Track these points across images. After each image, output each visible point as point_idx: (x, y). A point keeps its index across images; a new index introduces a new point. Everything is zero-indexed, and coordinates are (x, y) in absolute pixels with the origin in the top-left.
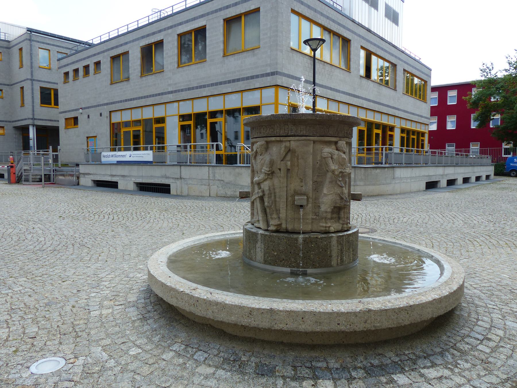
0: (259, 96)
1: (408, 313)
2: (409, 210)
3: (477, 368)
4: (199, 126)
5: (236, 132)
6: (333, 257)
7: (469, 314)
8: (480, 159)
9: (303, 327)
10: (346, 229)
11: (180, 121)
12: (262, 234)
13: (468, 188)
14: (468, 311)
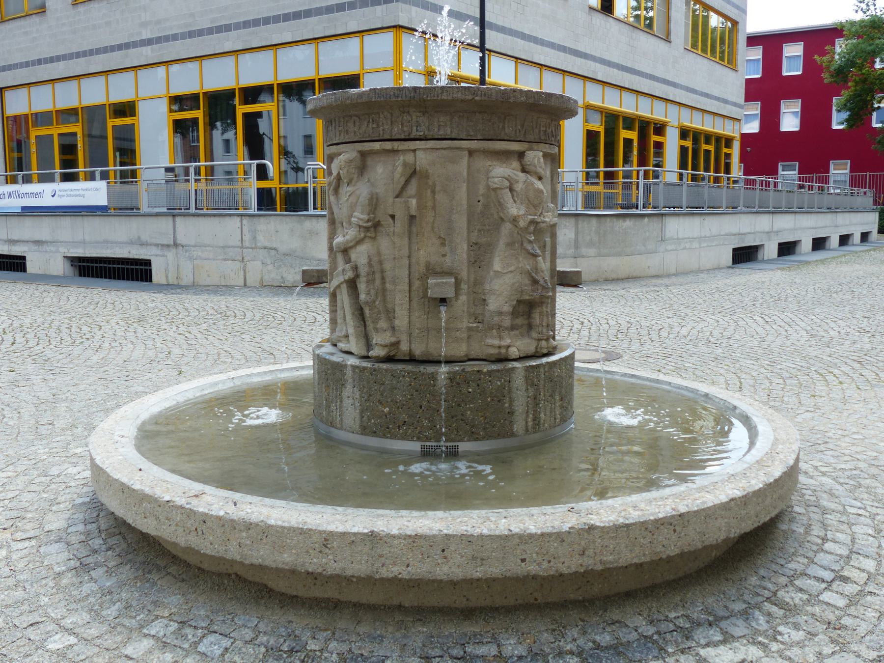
0: (357, 53)
1: (675, 531)
2: (693, 309)
3: (816, 639)
4: (218, 124)
5: (308, 138)
6: (517, 413)
7: (808, 528)
8: (849, 197)
9: (443, 571)
10: (545, 351)
11: (171, 111)
12: (354, 367)
13: (822, 261)
14: (805, 522)
